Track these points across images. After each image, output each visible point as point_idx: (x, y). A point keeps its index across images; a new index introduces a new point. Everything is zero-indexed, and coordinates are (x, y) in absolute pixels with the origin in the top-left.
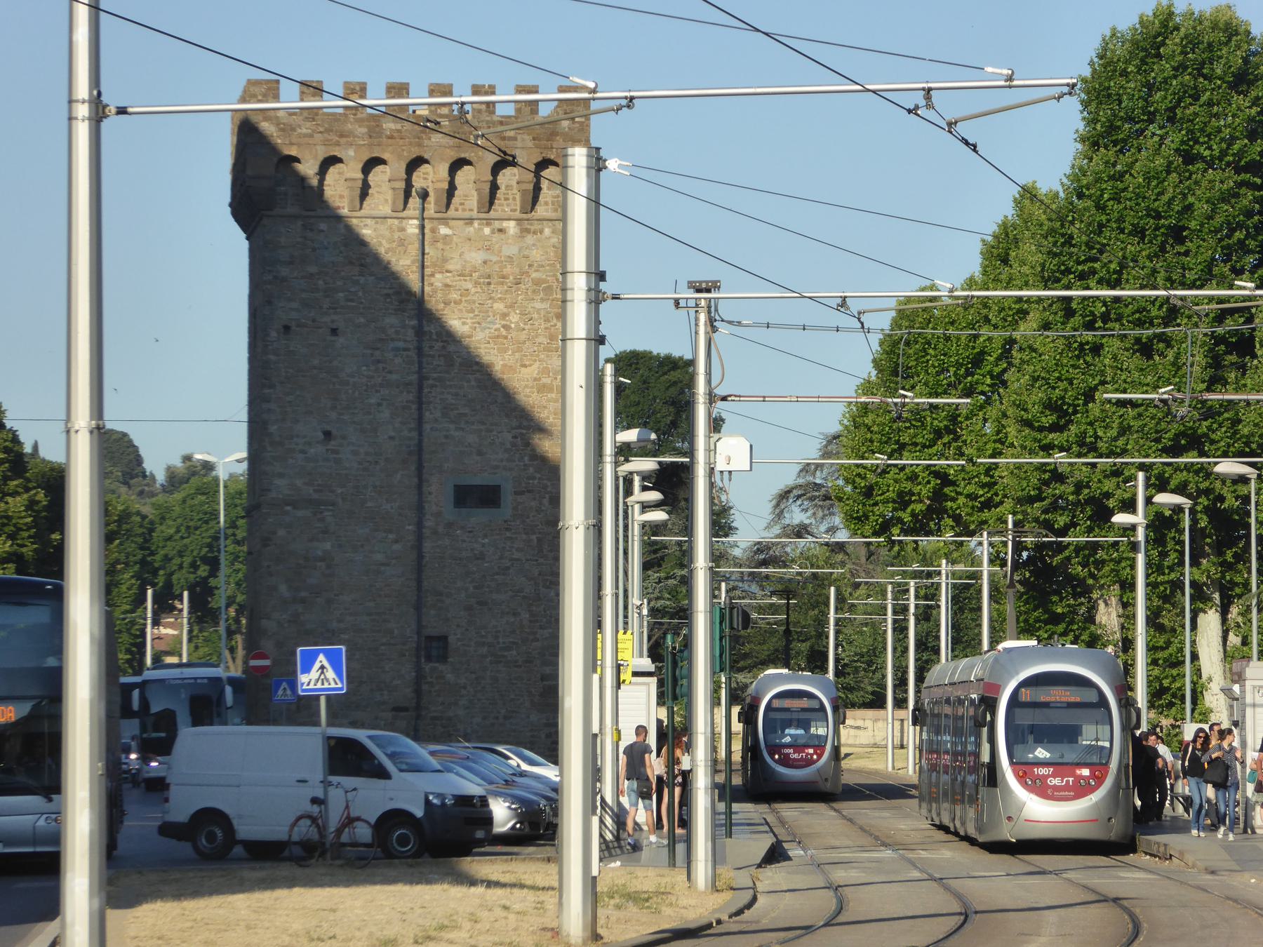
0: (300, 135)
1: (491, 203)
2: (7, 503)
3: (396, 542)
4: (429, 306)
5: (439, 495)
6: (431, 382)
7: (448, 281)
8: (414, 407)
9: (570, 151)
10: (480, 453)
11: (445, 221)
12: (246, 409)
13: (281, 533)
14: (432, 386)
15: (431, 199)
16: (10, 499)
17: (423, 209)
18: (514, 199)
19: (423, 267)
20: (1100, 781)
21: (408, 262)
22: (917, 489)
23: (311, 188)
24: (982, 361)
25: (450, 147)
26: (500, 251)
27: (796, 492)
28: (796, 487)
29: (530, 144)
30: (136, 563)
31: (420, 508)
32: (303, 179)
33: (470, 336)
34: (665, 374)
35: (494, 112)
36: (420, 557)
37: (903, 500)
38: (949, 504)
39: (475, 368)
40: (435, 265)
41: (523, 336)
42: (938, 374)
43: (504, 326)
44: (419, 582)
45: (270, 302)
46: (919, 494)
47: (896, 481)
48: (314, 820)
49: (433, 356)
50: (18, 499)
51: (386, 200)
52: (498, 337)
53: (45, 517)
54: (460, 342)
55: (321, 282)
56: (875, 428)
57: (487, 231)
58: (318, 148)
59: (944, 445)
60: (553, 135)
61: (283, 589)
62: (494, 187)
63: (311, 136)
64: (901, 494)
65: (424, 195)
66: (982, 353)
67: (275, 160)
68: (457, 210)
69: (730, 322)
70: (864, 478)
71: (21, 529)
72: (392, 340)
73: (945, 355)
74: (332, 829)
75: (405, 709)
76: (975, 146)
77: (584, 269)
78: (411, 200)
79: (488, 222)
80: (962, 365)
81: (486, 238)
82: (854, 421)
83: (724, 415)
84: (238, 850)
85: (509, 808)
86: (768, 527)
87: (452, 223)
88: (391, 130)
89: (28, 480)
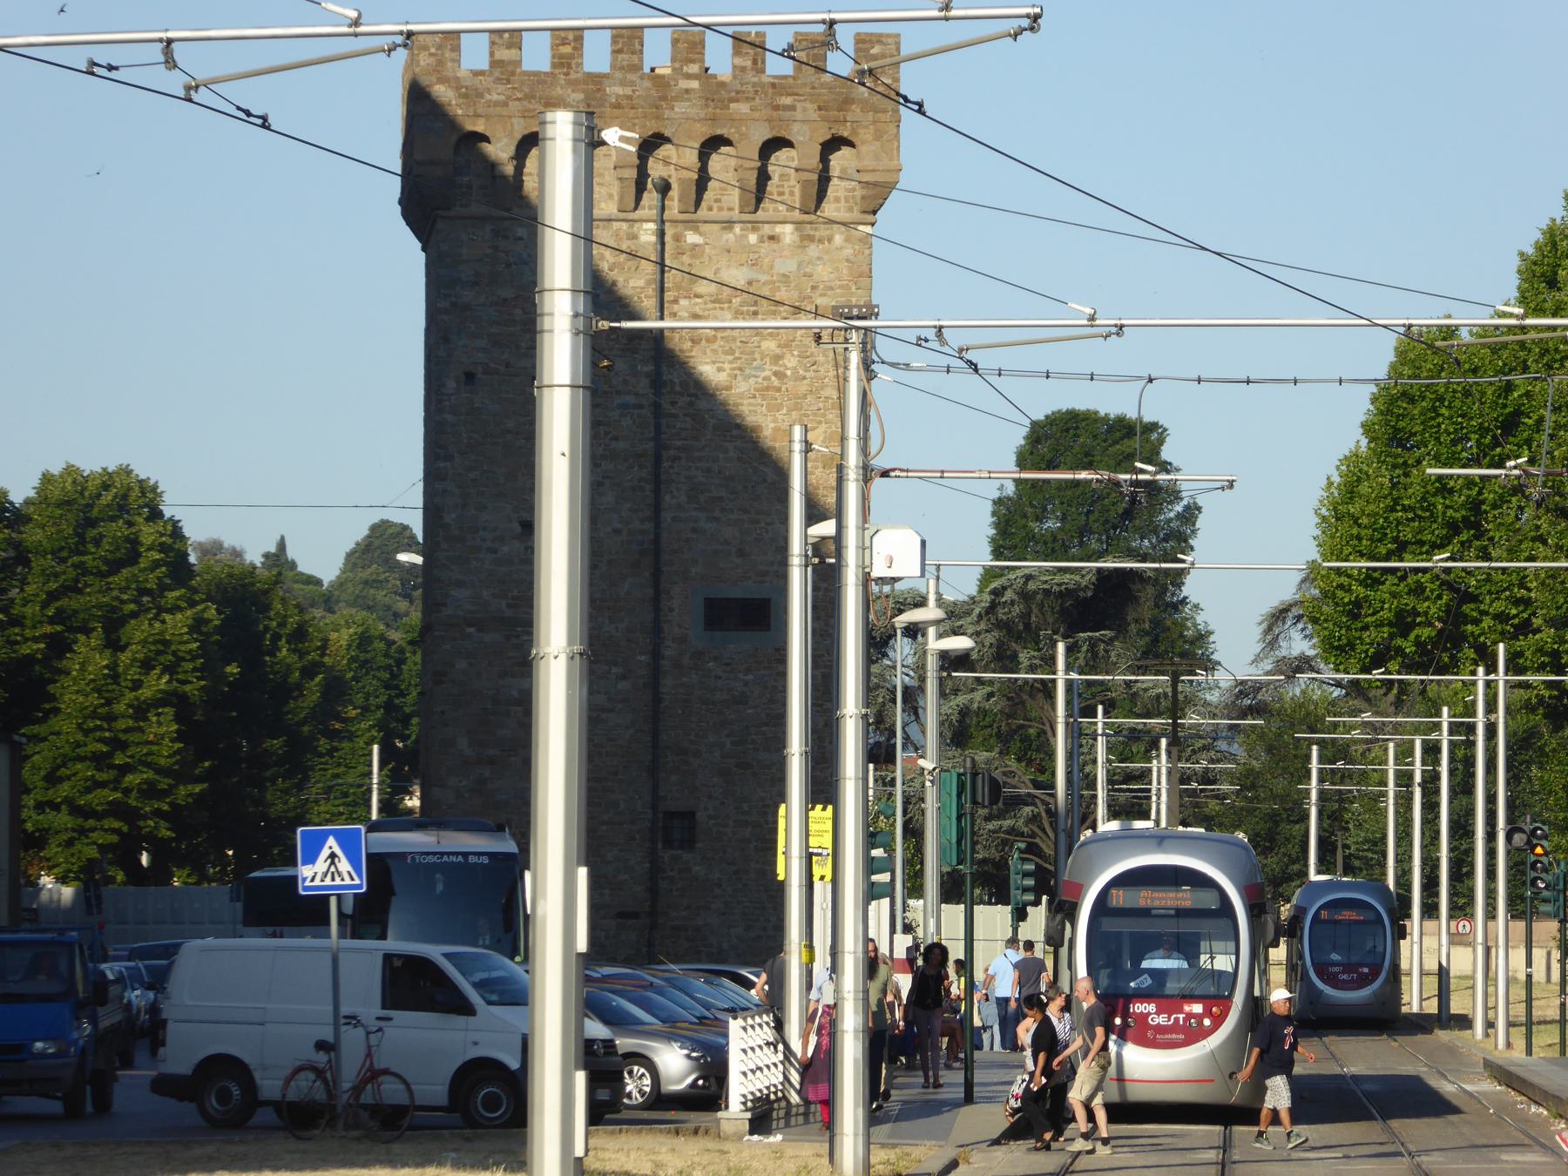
0: (489, 104)
1: (759, 200)
2: (163, 622)
3: (624, 677)
4: (671, 345)
5: (684, 613)
6: (672, 452)
7: (697, 310)
8: (649, 487)
9: (549, 116)
10: (741, 553)
11: (693, 225)
12: (420, 486)
13: (461, 664)
14: (676, 458)
15: (674, 193)
16: (168, 617)
17: (663, 208)
18: (792, 194)
19: (662, 290)
20: (1218, 1021)
21: (641, 283)
22: (1422, 607)
23: (505, 177)
24: (1517, 424)
25: (700, 121)
26: (772, 268)
27: (1296, 611)
28: (1296, 604)
29: (814, 116)
30: (378, 707)
31: (656, 630)
32: (492, 166)
33: (728, 388)
34: (1116, 442)
35: (763, 71)
36: (657, 699)
37: (1403, 623)
38: (1469, 627)
39: (734, 432)
40: (678, 287)
41: (803, 387)
42: (1454, 443)
43: (776, 374)
44: (655, 734)
45: (446, 340)
46: (1426, 613)
47: (1394, 595)
48: (319, 1073)
49: (675, 416)
50: (179, 616)
51: (611, 196)
52: (767, 388)
53: (217, 643)
54: (713, 396)
55: (518, 311)
56: (1364, 521)
57: (753, 238)
58: (515, 121)
59: (1462, 544)
60: (847, 102)
61: (463, 743)
62: (763, 177)
63: (505, 104)
64: (1400, 614)
65: (664, 188)
66: (1518, 413)
67: (454, 138)
68: (710, 209)
69: (893, 365)
70: (1349, 591)
71: (183, 659)
72: (618, 393)
73: (1463, 416)
74: (346, 1085)
75: (635, 915)
76: (920, 105)
77: (568, 286)
78: (645, 195)
79: (755, 226)
80: (1488, 430)
81: (751, 249)
82: (1335, 509)
83: (1200, 501)
84: (264, 1116)
85: (688, 1056)
86: (1256, 660)
87: (704, 227)
88: (618, 96)
89: (195, 591)
